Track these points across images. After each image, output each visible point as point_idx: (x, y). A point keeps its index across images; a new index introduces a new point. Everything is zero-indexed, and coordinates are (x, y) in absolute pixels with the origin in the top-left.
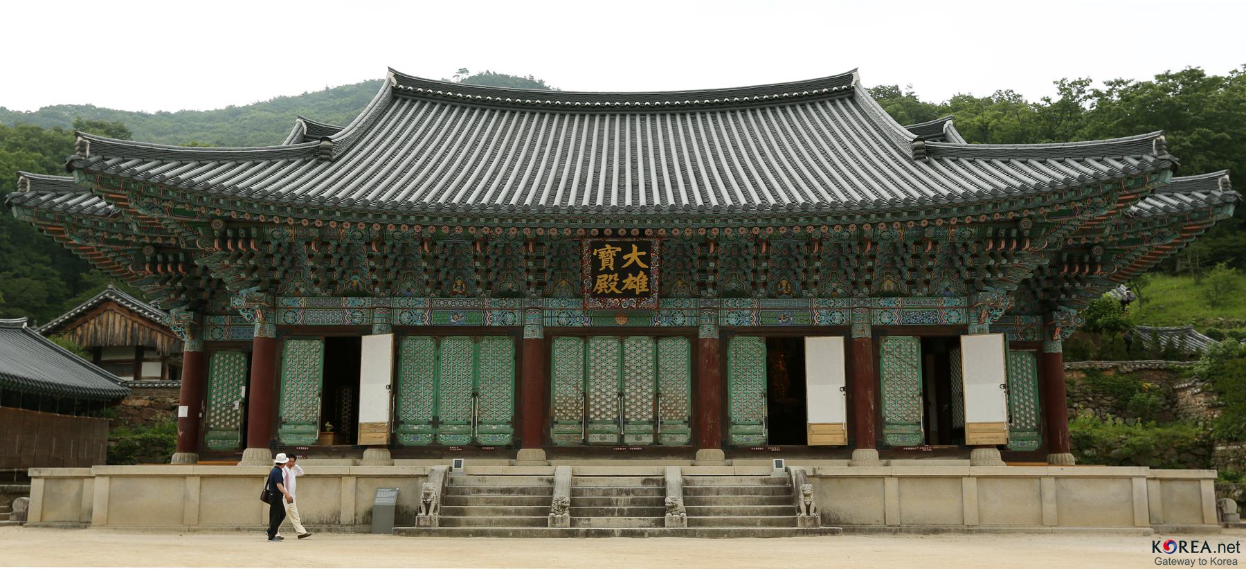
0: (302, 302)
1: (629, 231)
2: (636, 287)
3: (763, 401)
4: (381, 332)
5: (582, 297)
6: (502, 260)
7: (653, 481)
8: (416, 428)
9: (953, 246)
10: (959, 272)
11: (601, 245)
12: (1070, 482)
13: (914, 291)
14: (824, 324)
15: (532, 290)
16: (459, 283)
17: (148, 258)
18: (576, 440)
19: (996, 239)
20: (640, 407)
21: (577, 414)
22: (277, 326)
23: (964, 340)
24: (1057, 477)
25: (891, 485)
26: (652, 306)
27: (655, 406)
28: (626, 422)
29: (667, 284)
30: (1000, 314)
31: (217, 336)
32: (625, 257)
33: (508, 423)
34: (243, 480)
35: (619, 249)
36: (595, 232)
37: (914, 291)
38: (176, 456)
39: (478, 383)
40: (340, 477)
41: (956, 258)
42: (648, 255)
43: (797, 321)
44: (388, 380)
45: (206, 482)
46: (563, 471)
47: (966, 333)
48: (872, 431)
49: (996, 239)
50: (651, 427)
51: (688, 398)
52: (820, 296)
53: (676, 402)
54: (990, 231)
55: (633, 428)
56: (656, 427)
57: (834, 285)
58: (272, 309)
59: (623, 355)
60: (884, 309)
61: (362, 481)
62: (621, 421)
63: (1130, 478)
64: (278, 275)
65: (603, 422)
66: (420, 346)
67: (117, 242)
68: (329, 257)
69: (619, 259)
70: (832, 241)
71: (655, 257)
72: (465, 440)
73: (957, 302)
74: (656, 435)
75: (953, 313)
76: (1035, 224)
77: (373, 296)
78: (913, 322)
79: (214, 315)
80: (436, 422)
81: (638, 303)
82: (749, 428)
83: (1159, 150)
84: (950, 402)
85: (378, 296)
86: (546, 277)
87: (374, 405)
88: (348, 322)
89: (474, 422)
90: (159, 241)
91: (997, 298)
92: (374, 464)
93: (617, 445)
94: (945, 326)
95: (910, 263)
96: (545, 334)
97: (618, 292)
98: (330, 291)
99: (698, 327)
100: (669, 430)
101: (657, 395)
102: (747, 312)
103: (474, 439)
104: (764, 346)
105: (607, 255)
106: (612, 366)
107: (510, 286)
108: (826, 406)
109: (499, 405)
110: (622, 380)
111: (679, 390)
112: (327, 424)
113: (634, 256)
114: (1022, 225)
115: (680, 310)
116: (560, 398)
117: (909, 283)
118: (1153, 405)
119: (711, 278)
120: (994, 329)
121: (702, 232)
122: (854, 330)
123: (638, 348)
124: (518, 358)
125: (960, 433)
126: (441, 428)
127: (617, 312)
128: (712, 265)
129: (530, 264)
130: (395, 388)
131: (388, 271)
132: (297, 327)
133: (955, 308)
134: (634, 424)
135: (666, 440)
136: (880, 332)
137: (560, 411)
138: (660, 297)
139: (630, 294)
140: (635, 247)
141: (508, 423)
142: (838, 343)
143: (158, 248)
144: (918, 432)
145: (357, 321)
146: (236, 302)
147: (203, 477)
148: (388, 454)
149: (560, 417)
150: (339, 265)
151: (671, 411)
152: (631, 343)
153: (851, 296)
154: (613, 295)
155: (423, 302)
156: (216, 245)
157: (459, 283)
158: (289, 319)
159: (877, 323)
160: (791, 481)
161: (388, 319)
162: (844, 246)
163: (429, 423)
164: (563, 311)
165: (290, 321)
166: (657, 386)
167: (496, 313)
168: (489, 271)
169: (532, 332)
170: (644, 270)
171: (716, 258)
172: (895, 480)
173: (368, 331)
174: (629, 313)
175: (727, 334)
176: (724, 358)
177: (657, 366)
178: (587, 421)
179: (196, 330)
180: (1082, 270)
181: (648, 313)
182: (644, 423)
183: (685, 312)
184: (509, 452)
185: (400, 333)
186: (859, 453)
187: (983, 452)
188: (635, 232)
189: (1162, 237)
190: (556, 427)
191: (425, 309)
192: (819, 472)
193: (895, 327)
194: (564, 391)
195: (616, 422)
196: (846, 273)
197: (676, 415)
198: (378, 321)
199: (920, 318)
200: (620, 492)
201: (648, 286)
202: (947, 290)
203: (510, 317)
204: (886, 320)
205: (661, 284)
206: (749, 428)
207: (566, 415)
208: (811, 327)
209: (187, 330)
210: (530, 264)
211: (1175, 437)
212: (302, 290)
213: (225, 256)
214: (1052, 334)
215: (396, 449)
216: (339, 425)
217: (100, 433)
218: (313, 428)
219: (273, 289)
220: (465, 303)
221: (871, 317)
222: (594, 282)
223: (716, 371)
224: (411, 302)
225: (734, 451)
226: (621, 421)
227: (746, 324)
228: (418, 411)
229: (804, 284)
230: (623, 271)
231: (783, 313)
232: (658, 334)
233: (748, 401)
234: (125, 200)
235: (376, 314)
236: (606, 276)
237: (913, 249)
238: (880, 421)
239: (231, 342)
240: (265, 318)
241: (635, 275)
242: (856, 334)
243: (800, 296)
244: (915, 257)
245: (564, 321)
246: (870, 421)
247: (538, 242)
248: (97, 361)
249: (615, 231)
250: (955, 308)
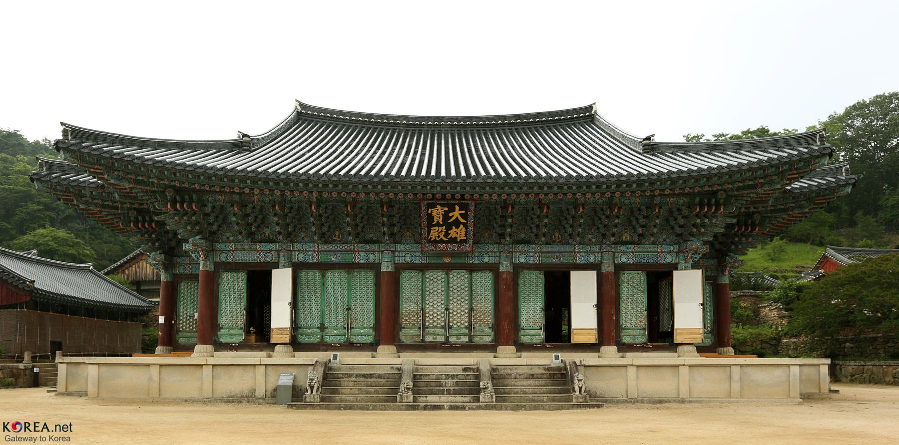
0: (231, 246)
1: (453, 195)
2: (458, 236)
3: (542, 314)
4: (285, 266)
5: (420, 243)
6: (366, 217)
7: (471, 369)
8: (309, 331)
10: (672, 228)
11: (433, 206)
12: (750, 369)
13: (643, 241)
14: (583, 262)
15: (387, 238)
16: (337, 233)
17: (132, 218)
18: (417, 340)
19: (701, 205)
20: (460, 319)
21: (417, 323)
22: (215, 263)
23: (675, 273)
24: (741, 366)
25: (632, 371)
26: (468, 249)
27: (470, 317)
28: (450, 328)
29: (478, 235)
30: (698, 257)
31: (182, 271)
32: (450, 215)
33: (371, 328)
34: (188, 368)
35: (446, 209)
36: (429, 196)
37: (643, 241)
38: (158, 349)
39: (348, 302)
40: (254, 365)
41: (671, 219)
42: (467, 213)
43: (565, 260)
44: (289, 299)
45: (163, 369)
46: (408, 360)
47: (676, 269)
48: (613, 334)
49: (701, 205)
50: (467, 331)
51: (492, 312)
52: (580, 243)
53: (484, 314)
54: (697, 200)
55: (455, 332)
56: (470, 331)
57: (590, 236)
58: (210, 252)
59: (448, 283)
60: (624, 253)
61: (270, 368)
62: (447, 327)
63: (788, 366)
64: (214, 228)
65: (435, 328)
66: (313, 276)
67: (108, 207)
68: (247, 215)
69: (446, 216)
70: (592, 206)
71: (471, 214)
72: (342, 339)
73: (671, 248)
74: (470, 336)
75: (668, 256)
76: (727, 195)
77: (278, 242)
78: (642, 261)
79: (178, 257)
80: (322, 328)
81: (459, 247)
82: (532, 332)
83: (821, 141)
84: (658, 315)
85: (282, 243)
86: (396, 229)
87: (280, 316)
88: (262, 260)
89: (349, 328)
90: (137, 206)
91: (697, 245)
92: (281, 355)
93: (444, 343)
94: (663, 264)
96: (395, 268)
98: (250, 239)
99: (499, 264)
100: (479, 333)
101: (471, 310)
102: (532, 254)
103: (348, 340)
104: (543, 277)
105: (438, 213)
106: (441, 290)
107: (371, 235)
108: (583, 317)
109: (365, 317)
110: (448, 300)
111: (486, 305)
112: (251, 329)
113: (456, 214)
114: (719, 195)
115: (487, 252)
116: (406, 312)
117: (640, 235)
118: (748, 316)
119: (509, 230)
120: (694, 267)
121: (504, 197)
122: (603, 267)
123: (459, 278)
124: (377, 285)
125: (670, 335)
126: (327, 331)
127: (444, 254)
128: (510, 220)
129: (385, 219)
130: (294, 305)
131: (288, 225)
133: (669, 253)
134: (455, 328)
135: (477, 340)
136: (620, 268)
137: (406, 320)
138: (474, 243)
139: (453, 240)
140: (457, 208)
141: (371, 328)
142: (592, 275)
143: (137, 210)
144: (643, 335)
145: (268, 259)
146: (187, 247)
147: (161, 365)
148: (291, 348)
149: (406, 325)
150: (255, 221)
151: (481, 321)
152: (453, 275)
153: (601, 243)
154: (442, 241)
155: (313, 247)
156: (169, 206)
157: (337, 233)
158: (223, 258)
160: (566, 369)
161: (289, 258)
162: (598, 210)
163: (318, 328)
164: (408, 253)
165: (224, 259)
166: (471, 303)
167: (362, 254)
168: (357, 225)
169: (386, 267)
170: (463, 223)
171: (512, 217)
172: (635, 368)
173: (277, 266)
174: (452, 254)
175: (518, 268)
176: (516, 285)
177: (471, 290)
178: (424, 327)
179: (168, 266)
180: (746, 229)
181: (465, 254)
182: (462, 328)
183: (490, 254)
184: (372, 347)
185: (297, 268)
186: (604, 349)
187: (685, 348)
188: (458, 196)
189: (801, 207)
190: (403, 331)
191: (314, 251)
192: (583, 363)
193: (630, 264)
194: (408, 306)
195: (444, 327)
196: (598, 228)
197: (484, 323)
199: (646, 259)
200: (448, 376)
201: (466, 236)
202: (665, 240)
203: (371, 257)
204: (624, 260)
205: (474, 235)
206: (532, 332)
207: (410, 323)
208: (575, 264)
209: (161, 267)
210: (385, 219)
211: (760, 334)
212: (231, 238)
213: (175, 215)
214: (723, 273)
215: (296, 345)
216: (258, 328)
217: (137, 332)
218: (241, 331)
219: (212, 238)
220: (341, 247)
221: (615, 258)
222: (429, 232)
223: (511, 294)
224: (305, 247)
225: (522, 347)
226: (447, 327)
227: (531, 262)
228: (310, 321)
229: (570, 235)
230: (448, 224)
231: (556, 255)
232: (472, 269)
233: (532, 314)
234: (102, 174)
235: (281, 254)
236: (437, 228)
238: (618, 327)
239: (191, 274)
240: (206, 259)
241: (457, 227)
242: (605, 269)
243: (567, 243)
244: (646, 217)
245: (408, 260)
246: (612, 327)
247: (390, 204)
248: (139, 291)
249: (444, 195)
250: (669, 253)
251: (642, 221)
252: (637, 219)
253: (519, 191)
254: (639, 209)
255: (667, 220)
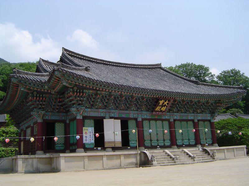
9: (103, 96)
31: (47, 118)
33: (63, 144)
47: (105, 119)
88: (100, 116)
95: (93, 100)
97: (159, 110)
113: (166, 103)
123: (159, 123)
132: (88, 116)
158: (86, 114)
159: (198, 119)
165: (86, 115)
193: (201, 120)
198: (107, 116)
232: (163, 120)
237: (94, 96)
245: (145, 117)
251: (93, 100)
252: (116, 101)
253: (127, 92)
254: (92, 95)
255: (88, 99)
